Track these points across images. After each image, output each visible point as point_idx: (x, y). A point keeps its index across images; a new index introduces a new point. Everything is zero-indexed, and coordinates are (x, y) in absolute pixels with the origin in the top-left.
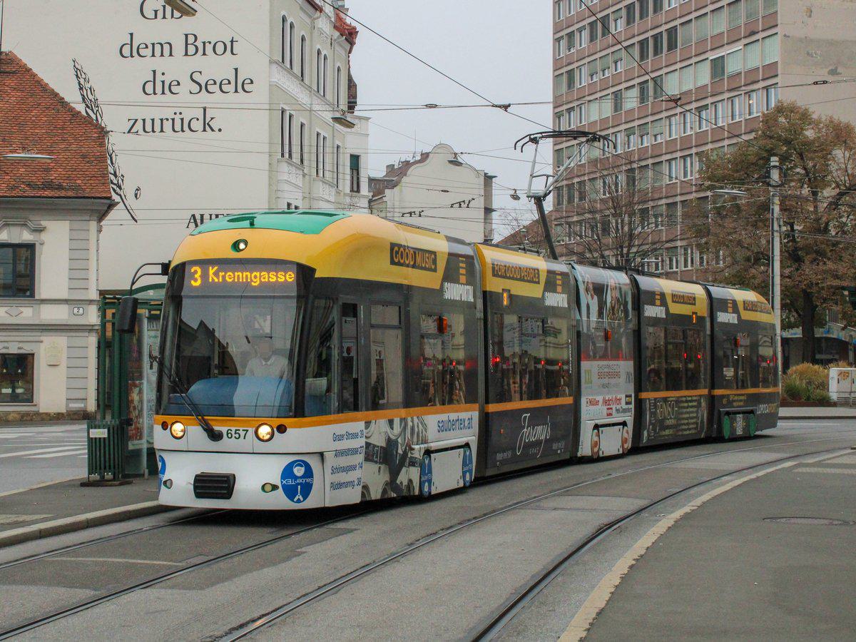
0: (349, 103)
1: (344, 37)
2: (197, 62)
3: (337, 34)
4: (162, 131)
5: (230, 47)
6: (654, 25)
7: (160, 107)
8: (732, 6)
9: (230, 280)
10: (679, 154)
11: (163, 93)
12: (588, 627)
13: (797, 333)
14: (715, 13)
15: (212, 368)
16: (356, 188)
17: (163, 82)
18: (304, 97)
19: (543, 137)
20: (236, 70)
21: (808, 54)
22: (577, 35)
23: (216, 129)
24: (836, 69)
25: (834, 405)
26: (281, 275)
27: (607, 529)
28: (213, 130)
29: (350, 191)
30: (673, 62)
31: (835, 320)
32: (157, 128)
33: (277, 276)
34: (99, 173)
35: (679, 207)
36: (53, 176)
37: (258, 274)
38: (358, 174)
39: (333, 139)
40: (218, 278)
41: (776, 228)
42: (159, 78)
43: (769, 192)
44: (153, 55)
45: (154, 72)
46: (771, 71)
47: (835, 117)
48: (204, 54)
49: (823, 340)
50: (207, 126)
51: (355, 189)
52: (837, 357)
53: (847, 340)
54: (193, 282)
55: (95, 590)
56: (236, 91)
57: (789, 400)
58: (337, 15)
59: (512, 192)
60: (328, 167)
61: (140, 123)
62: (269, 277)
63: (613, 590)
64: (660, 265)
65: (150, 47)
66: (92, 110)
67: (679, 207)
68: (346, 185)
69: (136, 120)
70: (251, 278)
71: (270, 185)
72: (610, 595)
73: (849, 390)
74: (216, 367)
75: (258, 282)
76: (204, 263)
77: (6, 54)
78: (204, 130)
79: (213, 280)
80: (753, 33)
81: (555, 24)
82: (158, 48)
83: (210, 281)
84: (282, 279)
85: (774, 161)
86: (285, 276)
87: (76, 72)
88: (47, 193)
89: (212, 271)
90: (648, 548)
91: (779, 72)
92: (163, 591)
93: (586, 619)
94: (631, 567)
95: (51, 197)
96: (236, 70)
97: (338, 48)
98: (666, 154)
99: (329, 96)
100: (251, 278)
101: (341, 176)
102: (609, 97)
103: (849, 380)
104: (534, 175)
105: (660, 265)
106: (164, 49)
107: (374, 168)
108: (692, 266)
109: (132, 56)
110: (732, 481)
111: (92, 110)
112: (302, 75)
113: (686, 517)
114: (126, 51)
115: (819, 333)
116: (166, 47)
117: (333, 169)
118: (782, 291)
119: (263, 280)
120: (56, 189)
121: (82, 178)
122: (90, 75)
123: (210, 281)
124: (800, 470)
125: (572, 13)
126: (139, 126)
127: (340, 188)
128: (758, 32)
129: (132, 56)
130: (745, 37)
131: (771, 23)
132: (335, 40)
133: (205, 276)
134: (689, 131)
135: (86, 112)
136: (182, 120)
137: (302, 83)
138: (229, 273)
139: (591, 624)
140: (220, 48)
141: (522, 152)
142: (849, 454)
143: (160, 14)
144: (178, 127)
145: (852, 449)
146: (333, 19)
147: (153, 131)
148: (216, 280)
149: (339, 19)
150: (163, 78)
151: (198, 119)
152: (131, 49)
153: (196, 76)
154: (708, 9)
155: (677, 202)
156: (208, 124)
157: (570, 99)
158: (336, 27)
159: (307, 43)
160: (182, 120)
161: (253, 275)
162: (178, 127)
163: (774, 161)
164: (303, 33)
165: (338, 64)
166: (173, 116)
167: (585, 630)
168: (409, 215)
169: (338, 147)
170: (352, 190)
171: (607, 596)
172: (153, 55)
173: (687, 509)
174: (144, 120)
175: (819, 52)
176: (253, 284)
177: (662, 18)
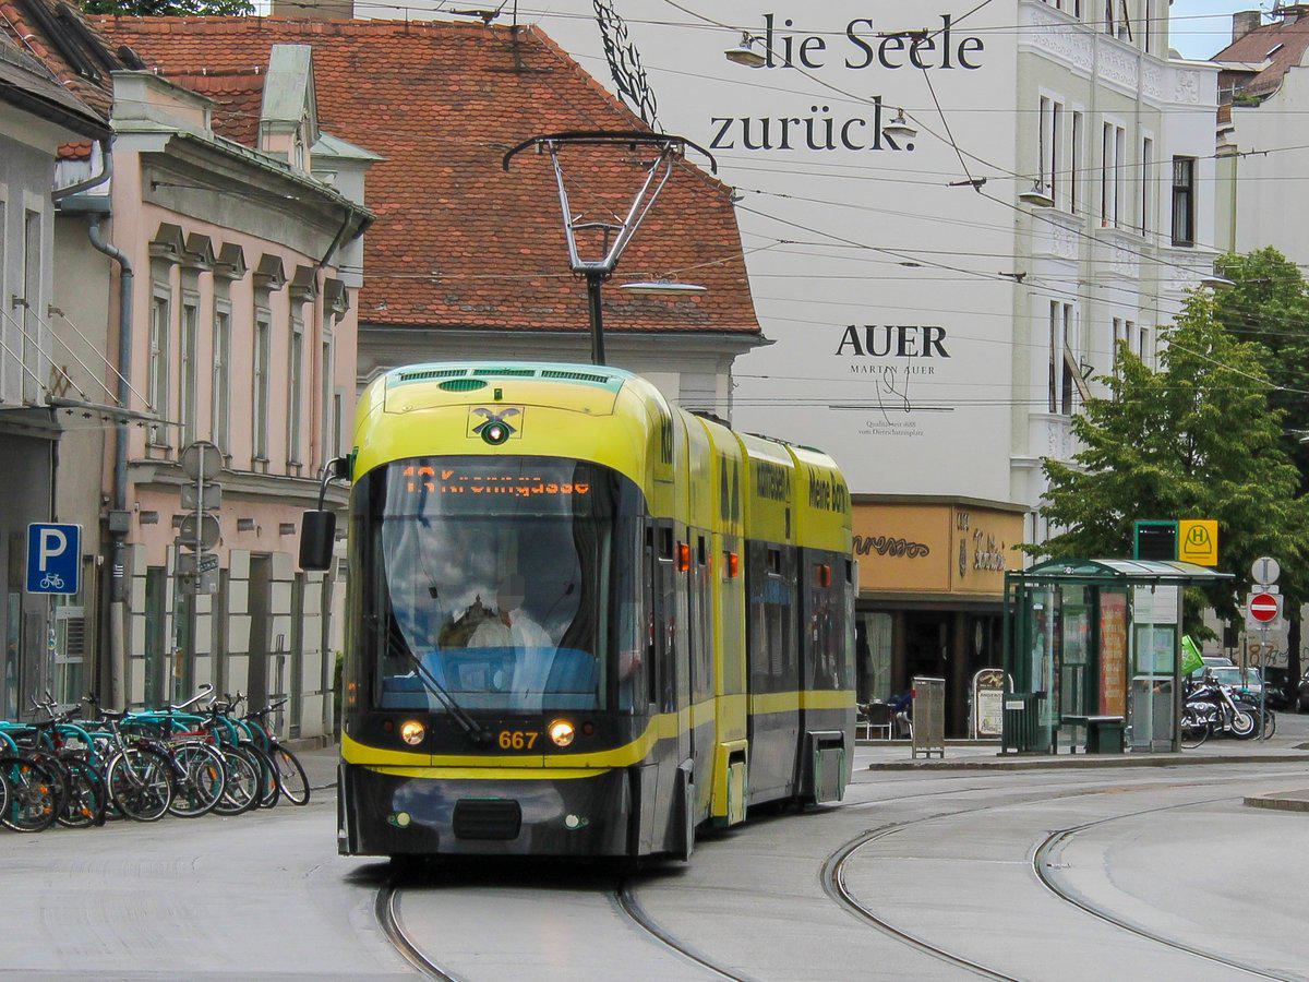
4: (785, 145)
17: (788, 41)
32: (775, 137)
39: (1137, 127)
45: (769, 18)
51: (1182, 236)
56: (946, 64)
61: (737, 127)
69: (729, 121)
77: (527, 33)
78: (877, 146)
87: (600, 13)
111: (634, 97)
126: (736, 131)
136: (829, 122)
144: (819, 138)
147: (766, 145)
151: (863, 123)
160: (829, 122)
162: (819, 138)
166: (810, 115)
174: (746, 122)
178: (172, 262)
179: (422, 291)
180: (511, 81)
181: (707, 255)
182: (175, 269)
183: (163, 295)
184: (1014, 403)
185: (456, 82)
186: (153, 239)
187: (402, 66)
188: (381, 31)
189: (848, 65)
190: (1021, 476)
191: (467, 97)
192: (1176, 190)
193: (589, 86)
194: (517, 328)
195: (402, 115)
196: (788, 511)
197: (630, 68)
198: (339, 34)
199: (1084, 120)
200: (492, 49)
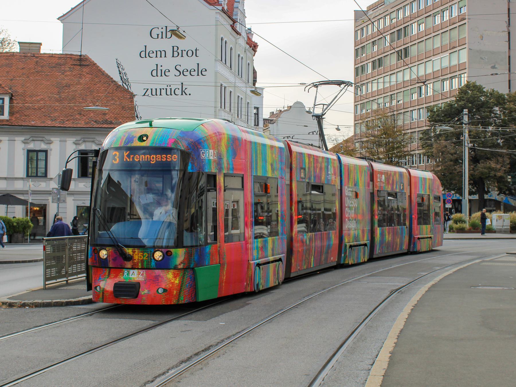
0: (253, 81)
1: (252, 48)
2: (178, 60)
4: (161, 95)
5: (195, 53)
7: (160, 82)
9: (137, 160)
11: (161, 76)
12: (397, 337)
13: (476, 197)
16: (257, 124)
17: (161, 70)
18: (231, 78)
19: (320, 84)
20: (198, 64)
21: (481, 58)
23: (188, 94)
25: (495, 232)
27: (394, 292)
28: (186, 94)
29: (254, 125)
31: (493, 190)
32: (158, 93)
34: (130, 116)
36: (107, 117)
38: (258, 116)
39: (246, 99)
40: (130, 159)
41: (466, 144)
42: (159, 68)
43: (463, 127)
44: (156, 57)
45: (157, 65)
47: (495, 90)
48: (182, 56)
49: (488, 201)
50: (183, 92)
51: (257, 124)
52: (495, 209)
53: (500, 200)
55: (153, 321)
56: (198, 75)
57: (472, 230)
58: (248, 37)
59: (337, 127)
60: (243, 113)
61: (150, 91)
63: (405, 320)
64: (407, 163)
65: (155, 52)
66: (126, 84)
68: (252, 122)
69: (148, 89)
70: (150, 158)
72: (404, 323)
73: (502, 225)
77: (84, 56)
78: (182, 94)
80: (454, 48)
82: (159, 53)
83: (125, 160)
85: (466, 111)
87: (118, 65)
88: (105, 126)
90: (418, 301)
92: (187, 321)
93: (395, 334)
94: (412, 310)
95: (107, 128)
96: (198, 64)
97: (248, 53)
100: (150, 158)
101: (249, 117)
103: (502, 220)
104: (316, 104)
105: (407, 163)
106: (162, 53)
107: (265, 114)
109: (146, 57)
110: (451, 269)
111: (126, 84)
112: (231, 67)
113: (433, 286)
114: (143, 54)
115: (486, 197)
116: (163, 53)
117: (246, 114)
118: (469, 177)
120: (109, 124)
121: (122, 118)
122: (124, 67)
123: (125, 160)
124: (484, 264)
126: (149, 92)
127: (249, 123)
129: (146, 57)
132: (247, 49)
135: (123, 85)
136: (171, 89)
137: (231, 71)
139: (398, 336)
140: (190, 53)
141: (305, 91)
142: (506, 256)
143: (160, 36)
144: (169, 93)
145: (507, 253)
146: (246, 39)
147: (156, 95)
148: (128, 160)
149: (249, 39)
150: (161, 68)
151: (179, 89)
152: (145, 54)
153: (178, 67)
156: (184, 91)
158: (247, 43)
159: (233, 51)
160: (171, 89)
161: (151, 157)
162: (169, 93)
163: (466, 111)
165: (248, 62)
166: (167, 87)
167: (396, 339)
168: (287, 138)
169: (248, 103)
170: (255, 125)
171: (403, 323)
172: (156, 57)
173: (432, 283)
174: (152, 89)
176: (152, 162)
177: (408, 39)
179: (45, 118)
180: (79, 67)
181: (125, 109)
185: (63, 68)
187: (50, 64)
188: (45, 56)
189: (175, 76)
191: (65, 71)
193: (99, 69)
194: (69, 127)
195: (48, 75)
197: (125, 77)
198: (34, 56)
200: (74, 60)
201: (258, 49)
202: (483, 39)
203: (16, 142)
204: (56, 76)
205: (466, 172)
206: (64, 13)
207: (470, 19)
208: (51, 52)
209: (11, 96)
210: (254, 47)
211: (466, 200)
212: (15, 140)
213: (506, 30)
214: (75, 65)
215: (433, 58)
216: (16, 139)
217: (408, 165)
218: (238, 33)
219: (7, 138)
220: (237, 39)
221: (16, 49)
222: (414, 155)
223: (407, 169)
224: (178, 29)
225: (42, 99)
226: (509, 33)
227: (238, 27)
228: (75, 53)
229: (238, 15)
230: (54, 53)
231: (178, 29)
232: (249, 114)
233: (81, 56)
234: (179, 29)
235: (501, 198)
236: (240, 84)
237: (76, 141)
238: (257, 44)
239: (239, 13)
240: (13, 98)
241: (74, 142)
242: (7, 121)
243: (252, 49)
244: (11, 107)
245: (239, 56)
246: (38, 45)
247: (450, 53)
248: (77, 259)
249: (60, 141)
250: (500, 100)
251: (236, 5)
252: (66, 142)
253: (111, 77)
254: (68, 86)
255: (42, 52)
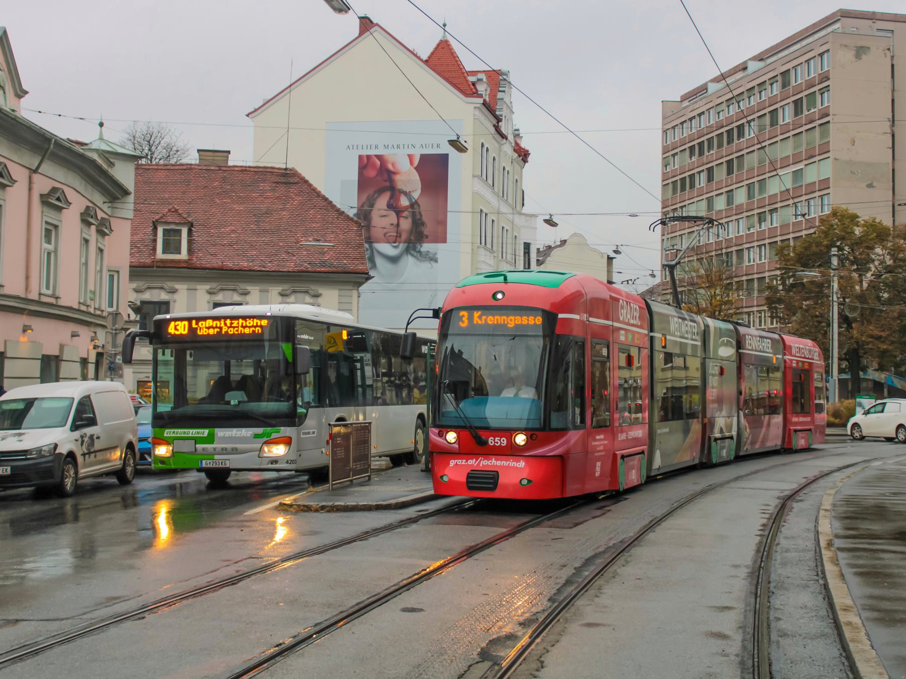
3: (516, 155)
6: (737, 150)
8: (796, 136)
10: (755, 244)
14: (784, 141)
15: (470, 389)
18: (494, 201)
21: (852, 172)
22: (780, 112)
24: (872, 183)
26: (531, 318)
30: (751, 176)
33: (528, 320)
35: (756, 281)
37: (513, 318)
38: (529, 256)
41: (835, 299)
46: (825, 184)
54: (461, 323)
59: (651, 272)
62: (522, 320)
67: (756, 281)
71: (472, 264)
74: (474, 389)
75: (513, 324)
76: (471, 308)
77: (291, 170)
79: (477, 322)
81: (664, 147)
83: (475, 322)
84: (532, 322)
86: (535, 320)
89: (476, 314)
91: (831, 185)
98: (746, 243)
99: (510, 200)
102: (744, 188)
108: (765, 325)
119: (517, 323)
125: (676, 139)
128: (815, 156)
130: (805, 160)
131: (825, 150)
132: (515, 159)
133: (471, 318)
134: (813, 214)
138: (490, 317)
146: (513, 145)
149: (517, 144)
154: (803, 129)
155: (765, 277)
157: (674, 202)
158: (515, 150)
164: (494, 155)
165: (516, 177)
169: (516, 237)
175: (860, 171)
176: (509, 325)
178: (93, 224)
182: (93, 228)
183: (87, 237)
184: (472, 243)
186: (82, 212)
187: (243, 180)
188: (236, 169)
190: (544, 665)
192: (525, 253)
194: (273, 271)
196: (76, 379)
199: (495, 223)
201: (530, 159)
202: (855, 144)
203: (198, 292)
204: (252, 198)
205: (834, 339)
206: (256, 108)
207: (835, 115)
208: (244, 164)
209: (190, 226)
210: (523, 155)
211: (835, 380)
212: (196, 289)
213: (889, 131)
214: (278, 183)
215: (781, 172)
216: (198, 287)
217: (754, 326)
218: (503, 136)
219: (185, 287)
220: (502, 145)
221: (192, 158)
222: (752, 314)
223: (780, 335)
224: (458, 138)
225: (233, 231)
226: (893, 136)
227: (503, 129)
228: (277, 166)
229: (504, 110)
230: (248, 165)
231: (458, 138)
232: (517, 253)
233: (286, 169)
234: (460, 139)
235: (881, 377)
236: (504, 209)
237: (283, 290)
238: (528, 151)
239: (505, 107)
240: (193, 229)
241: (279, 293)
242: (185, 261)
243: (522, 159)
244: (190, 242)
245: (504, 169)
246: (225, 154)
247: (806, 165)
248: (341, 450)
249: (261, 291)
250: (879, 234)
251: (500, 95)
252: (268, 292)
253: (330, 199)
254: (268, 213)
255: (230, 163)
